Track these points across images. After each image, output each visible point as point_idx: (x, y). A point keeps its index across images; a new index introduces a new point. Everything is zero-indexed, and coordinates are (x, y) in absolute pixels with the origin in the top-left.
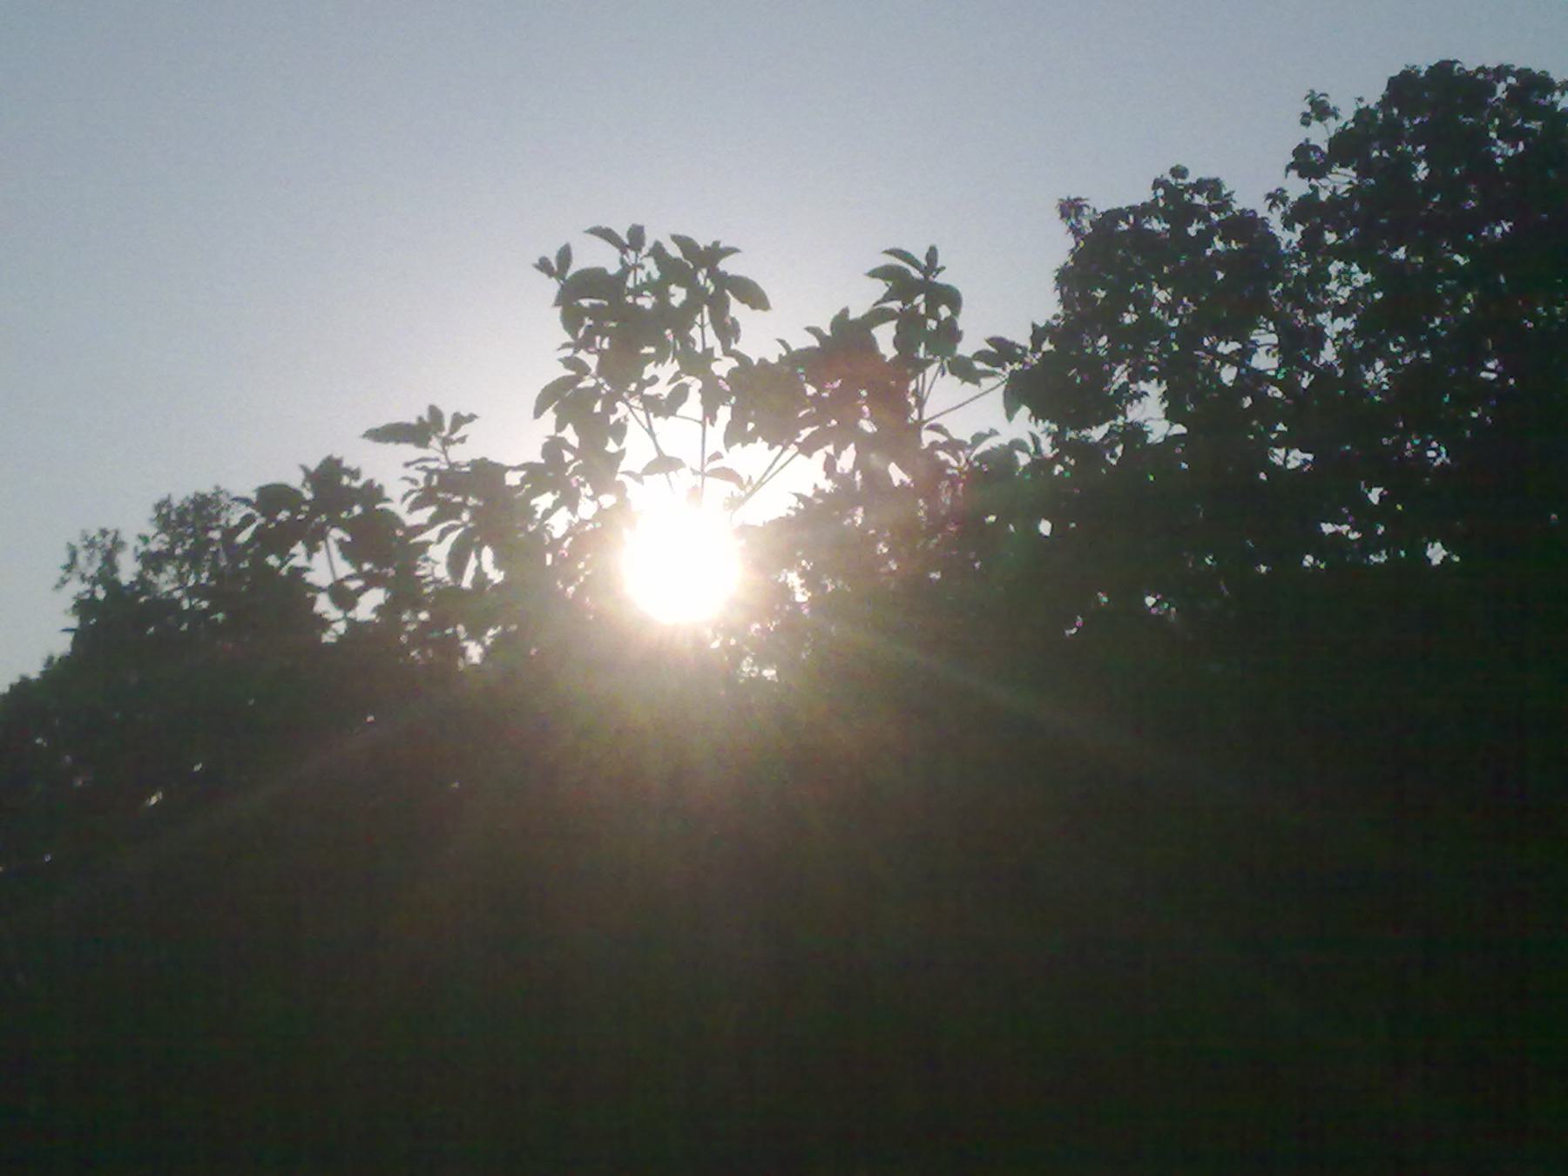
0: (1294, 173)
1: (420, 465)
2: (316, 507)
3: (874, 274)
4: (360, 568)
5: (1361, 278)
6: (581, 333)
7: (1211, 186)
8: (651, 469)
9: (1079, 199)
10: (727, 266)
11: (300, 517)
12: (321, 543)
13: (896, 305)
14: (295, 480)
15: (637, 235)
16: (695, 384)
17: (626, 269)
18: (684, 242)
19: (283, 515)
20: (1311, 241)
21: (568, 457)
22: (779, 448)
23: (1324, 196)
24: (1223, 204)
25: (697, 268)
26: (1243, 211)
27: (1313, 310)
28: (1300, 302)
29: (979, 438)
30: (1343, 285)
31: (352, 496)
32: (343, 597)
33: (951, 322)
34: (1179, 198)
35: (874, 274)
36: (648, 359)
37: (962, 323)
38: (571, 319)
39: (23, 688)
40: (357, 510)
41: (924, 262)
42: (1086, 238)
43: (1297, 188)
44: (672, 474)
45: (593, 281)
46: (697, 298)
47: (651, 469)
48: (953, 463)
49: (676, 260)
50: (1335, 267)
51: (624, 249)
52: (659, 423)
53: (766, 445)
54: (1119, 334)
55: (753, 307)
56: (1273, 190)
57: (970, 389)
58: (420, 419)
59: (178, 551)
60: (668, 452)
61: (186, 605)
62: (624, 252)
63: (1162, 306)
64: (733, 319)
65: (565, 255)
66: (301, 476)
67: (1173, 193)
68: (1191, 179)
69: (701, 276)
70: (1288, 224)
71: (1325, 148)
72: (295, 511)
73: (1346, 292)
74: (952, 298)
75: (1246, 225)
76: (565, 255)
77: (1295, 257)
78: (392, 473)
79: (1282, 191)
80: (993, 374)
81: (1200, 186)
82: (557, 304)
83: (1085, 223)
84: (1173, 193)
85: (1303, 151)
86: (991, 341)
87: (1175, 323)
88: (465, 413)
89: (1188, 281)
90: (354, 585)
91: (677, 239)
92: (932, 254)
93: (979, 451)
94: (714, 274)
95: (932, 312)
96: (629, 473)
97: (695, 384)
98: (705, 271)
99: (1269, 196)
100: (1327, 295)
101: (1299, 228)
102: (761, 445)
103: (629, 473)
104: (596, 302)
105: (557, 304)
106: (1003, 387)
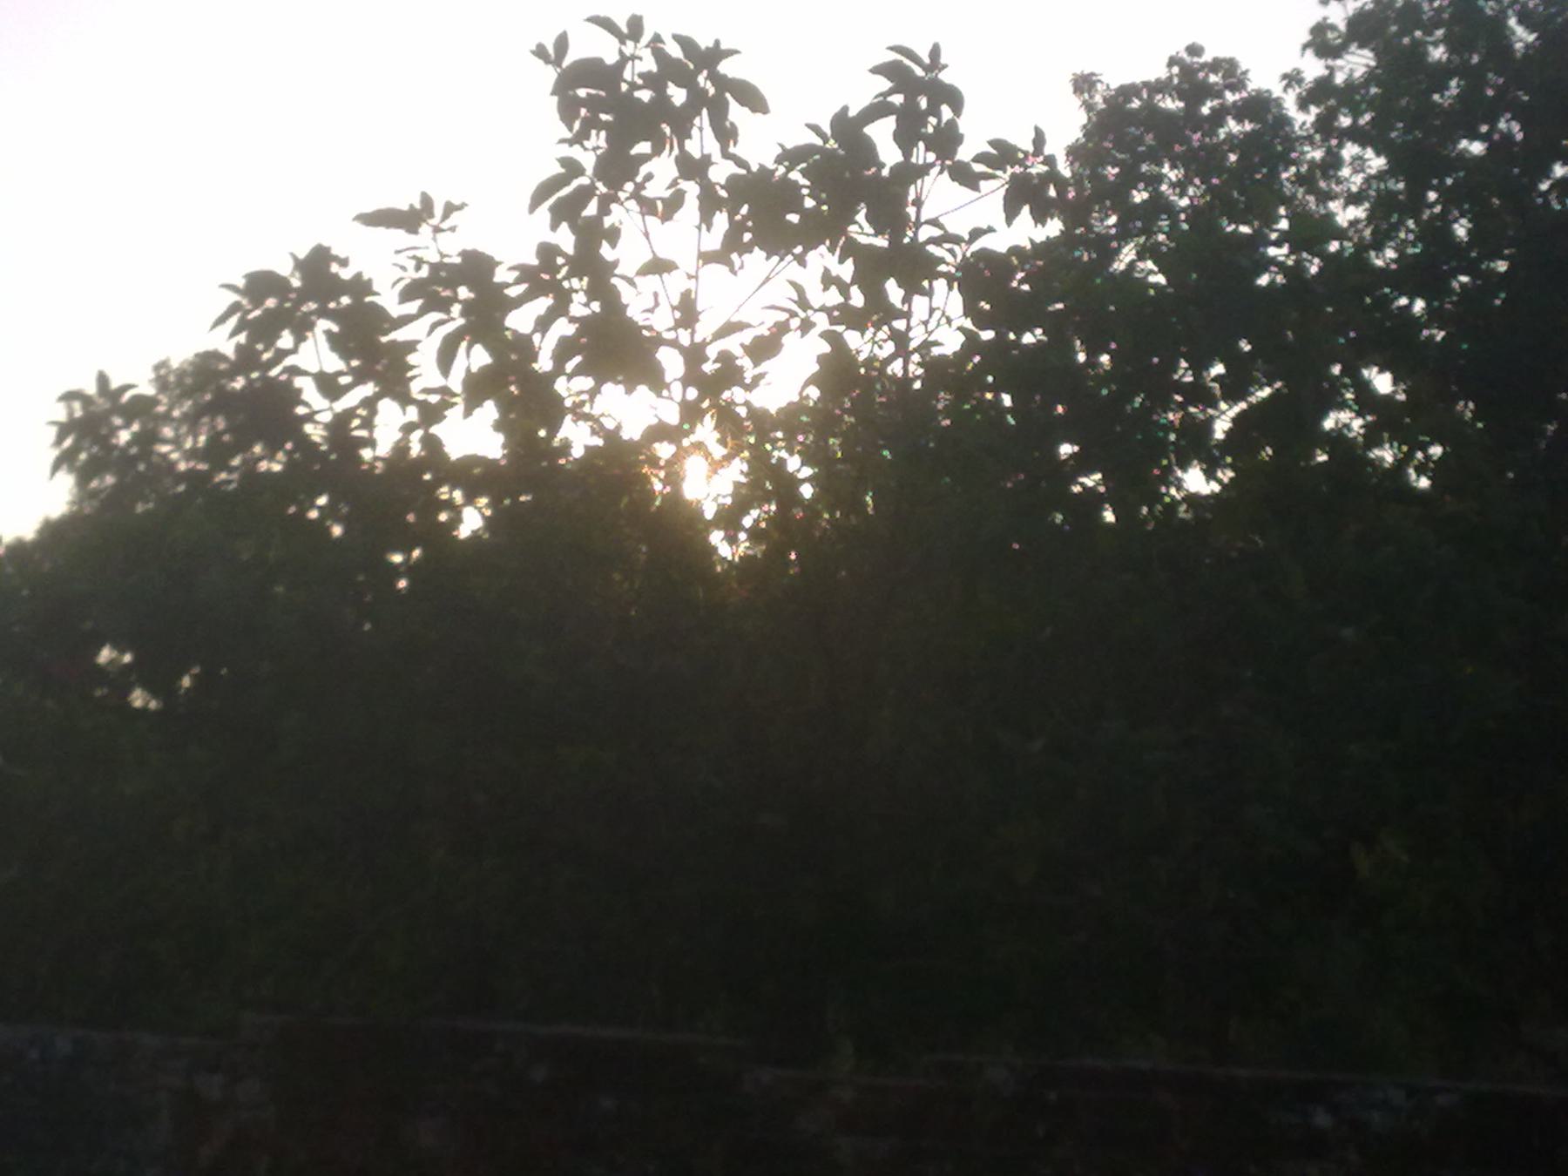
0: (1309, 53)
1: (411, 253)
2: (304, 295)
3: (876, 70)
4: (348, 364)
5: (1377, 163)
6: (577, 125)
7: (1227, 67)
8: (647, 270)
9: (1093, 74)
10: (726, 68)
11: (288, 305)
12: (309, 334)
13: (898, 99)
14: (284, 268)
15: (636, 26)
16: (692, 189)
17: (624, 60)
18: (685, 43)
19: (271, 303)
20: (1325, 126)
21: (560, 261)
22: (776, 259)
23: (1339, 79)
24: (1237, 83)
25: (698, 71)
26: (1259, 92)
27: (1328, 196)
28: (1312, 189)
29: (976, 234)
30: (1355, 172)
31: (339, 287)
32: (329, 385)
33: (952, 125)
34: (1194, 78)
35: (876, 70)
36: (645, 158)
37: (964, 124)
38: (568, 110)
39: (19, 551)
40: (345, 300)
41: (927, 61)
42: (1100, 113)
43: (1314, 68)
44: (665, 275)
45: (590, 71)
46: (697, 99)
47: (647, 270)
48: (949, 258)
49: (679, 60)
50: (1350, 150)
51: (622, 39)
52: (652, 221)
53: (764, 254)
54: (1129, 214)
55: (754, 110)
56: (1288, 70)
57: (965, 193)
58: (411, 206)
59: (176, 413)
60: (661, 255)
61: (182, 466)
62: (622, 42)
63: (1173, 185)
64: (732, 124)
65: (562, 43)
66: (290, 264)
67: (1188, 72)
68: (1207, 57)
69: (701, 79)
70: (1303, 104)
71: (1342, 27)
72: (283, 298)
73: (1358, 179)
74: (954, 99)
75: (1259, 107)
76: (562, 43)
77: (1309, 139)
78: (382, 265)
79: (1299, 72)
80: (993, 177)
81: (1215, 66)
82: (553, 93)
83: (1098, 99)
84: (1188, 72)
85: (1320, 30)
86: (992, 143)
87: (1184, 202)
88: (457, 202)
89: (1201, 163)
90: (345, 380)
91: (678, 39)
92: (935, 52)
93: (976, 247)
94: (715, 78)
95: (934, 110)
96: (623, 277)
97: (692, 189)
98: (705, 73)
99: (1285, 76)
100: (1339, 182)
101: (1314, 110)
102: (759, 254)
103: (623, 277)
104: (593, 92)
105: (553, 93)
106: (1002, 192)
